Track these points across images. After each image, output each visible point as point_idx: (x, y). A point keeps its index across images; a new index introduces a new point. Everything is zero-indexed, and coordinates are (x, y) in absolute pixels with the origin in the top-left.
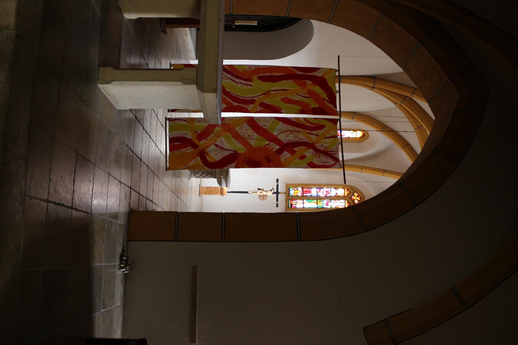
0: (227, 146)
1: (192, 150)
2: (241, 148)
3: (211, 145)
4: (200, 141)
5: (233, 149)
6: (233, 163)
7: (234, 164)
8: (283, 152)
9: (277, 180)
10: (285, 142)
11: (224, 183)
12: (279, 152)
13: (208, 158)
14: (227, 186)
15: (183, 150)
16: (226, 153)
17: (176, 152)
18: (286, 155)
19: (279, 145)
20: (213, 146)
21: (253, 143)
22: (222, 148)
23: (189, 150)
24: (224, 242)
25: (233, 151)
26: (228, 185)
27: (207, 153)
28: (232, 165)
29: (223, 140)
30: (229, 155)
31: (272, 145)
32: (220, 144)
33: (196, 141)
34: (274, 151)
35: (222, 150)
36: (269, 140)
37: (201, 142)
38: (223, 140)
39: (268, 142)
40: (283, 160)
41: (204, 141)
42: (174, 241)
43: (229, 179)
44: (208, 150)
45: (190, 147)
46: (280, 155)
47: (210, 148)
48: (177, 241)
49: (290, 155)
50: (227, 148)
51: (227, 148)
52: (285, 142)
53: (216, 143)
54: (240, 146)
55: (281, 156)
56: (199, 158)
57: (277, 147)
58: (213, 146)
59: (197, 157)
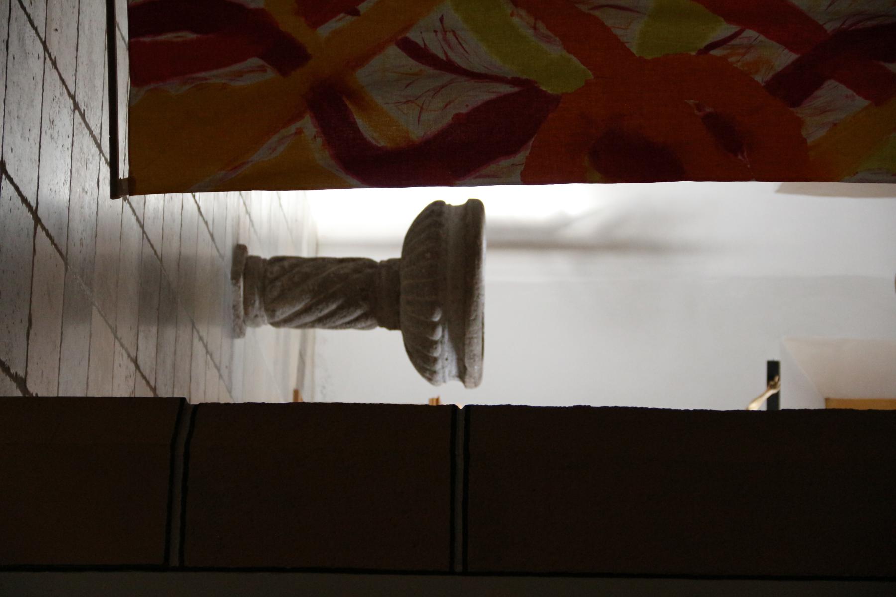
0: (478, 53)
1: (271, 74)
2: (557, 67)
3: (380, 48)
4: (315, 24)
5: (510, 69)
6: (511, 151)
7: (521, 157)
8: (818, 84)
9: (773, 369)
10: (830, 27)
11: (445, 354)
12: (795, 86)
13: (361, 123)
14: (462, 374)
15: (216, 76)
16: (479, 95)
17: (174, 88)
18: (835, 104)
19: (790, 46)
20: (393, 55)
21: (632, 34)
22: (448, 66)
23: (251, 74)
24: (465, 573)
25: (514, 81)
26: (473, 369)
27: (358, 97)
28: (504, 163)
29: (454, 18)
30: (488, 104)
31: (749, 48)
32: (436, 47)
33: (291, 24)
34: (760, 78)
35: (448, 77)
36: (730, 18)
37: (325, 31)
38: (454, 18)
39: (724, 30)
40: (815, 131)
41: (340, 23)
42: (164, 567)
43: (476, 327)
44: (363, 76)
45: (254, 61)
46: (797, 103)
47: (376, 62)
48: (182, 568)
49: (861, 102)
50: (478, 68)
51: (475, 64)
52: (830, 27)
53: (413, 35)
54: (555, 51)
55: (803, 112)
56: (308, 125)
57: (783, 58)
58: (393, 51)
59: (299, 116)
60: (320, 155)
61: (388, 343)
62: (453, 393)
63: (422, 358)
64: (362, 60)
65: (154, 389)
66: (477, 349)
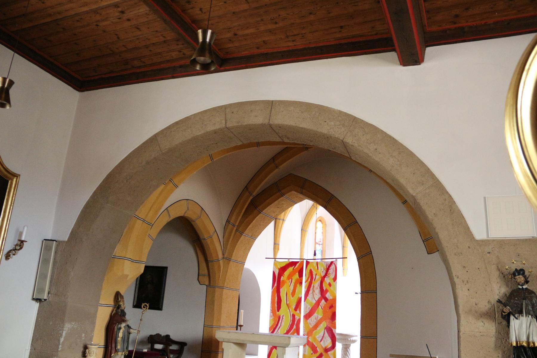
0: (322, 334)
11: (354, 338)
12: (326, 300)
16: (326, 334)
20: (322, 343)
22: (323, 337)
32: (321, 338)
33: (318, 354)
39: (320, 307)
41: (318, 349)
44: (324, 347)
54: (322, 325)
56: (329, 353)
57: (323, 301)
60: (332, 352)
61: (352, 345)
62: (358, 339)
63: (354, 341)
64: (322, 347)
65: (139, 262)
66: (257, 119)
